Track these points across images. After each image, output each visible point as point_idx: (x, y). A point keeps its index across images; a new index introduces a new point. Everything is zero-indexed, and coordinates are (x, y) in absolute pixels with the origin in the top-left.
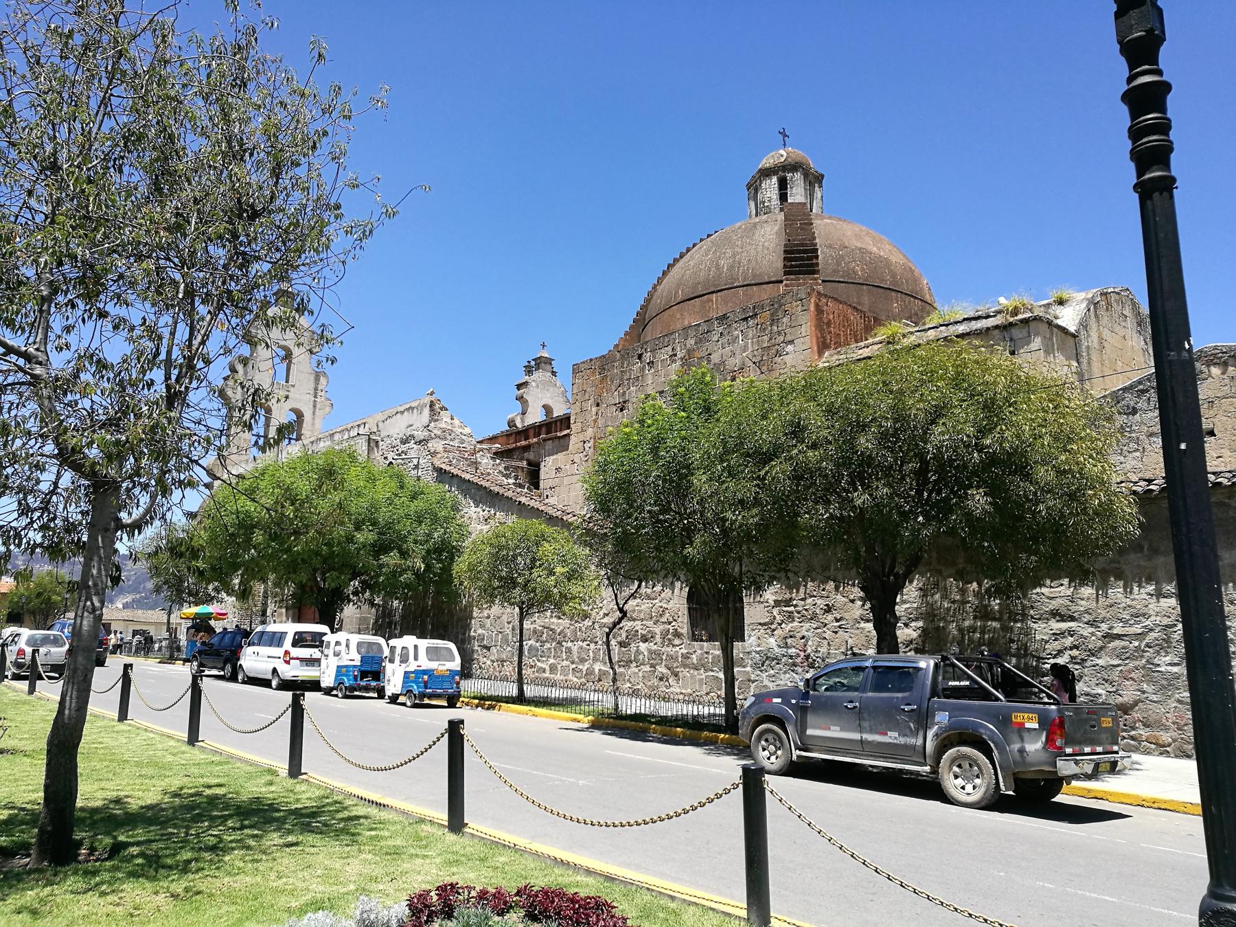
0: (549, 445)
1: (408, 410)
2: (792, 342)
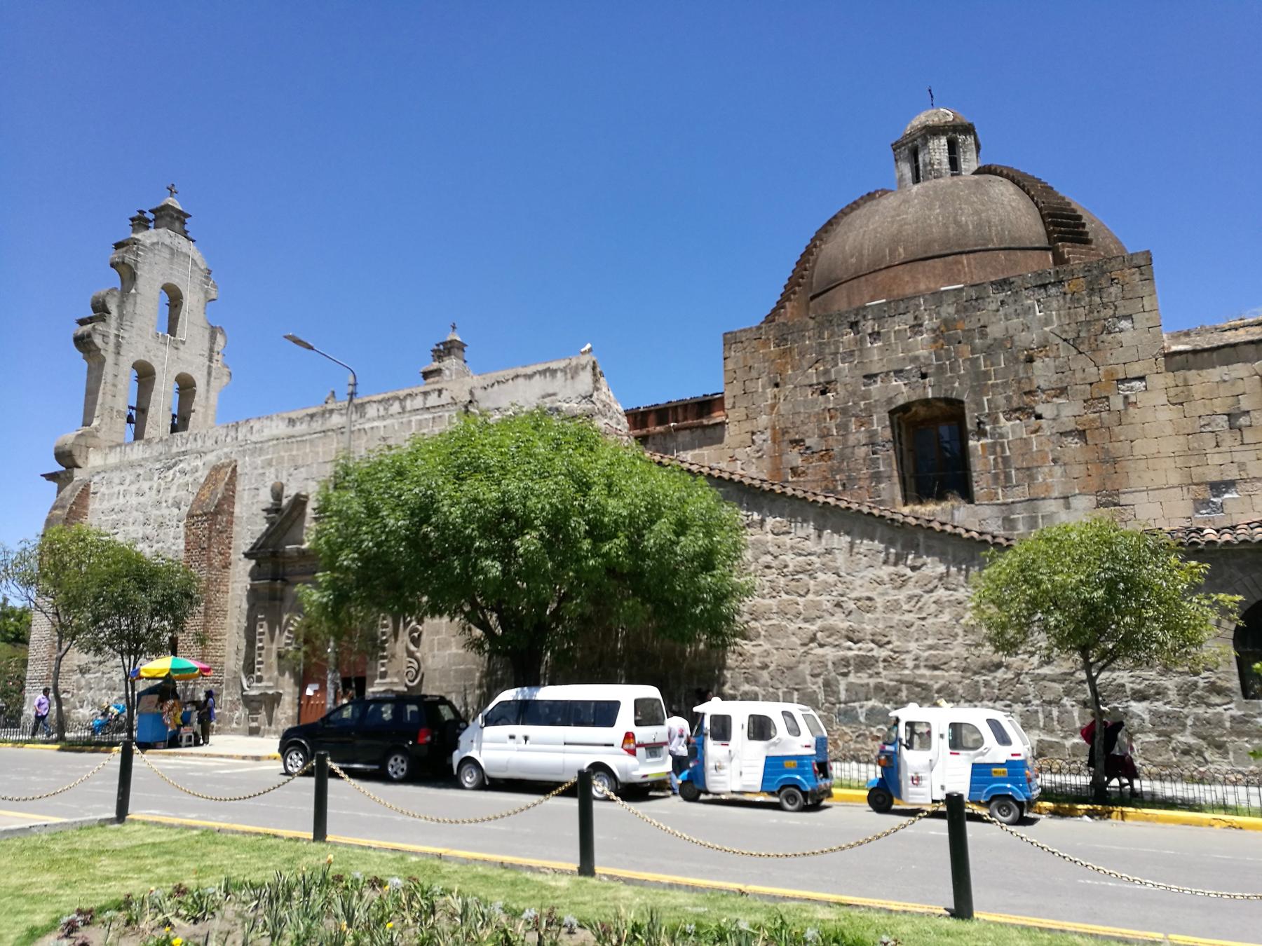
0: (684, 436)
1: (543, 373)
2: (1129, 317)
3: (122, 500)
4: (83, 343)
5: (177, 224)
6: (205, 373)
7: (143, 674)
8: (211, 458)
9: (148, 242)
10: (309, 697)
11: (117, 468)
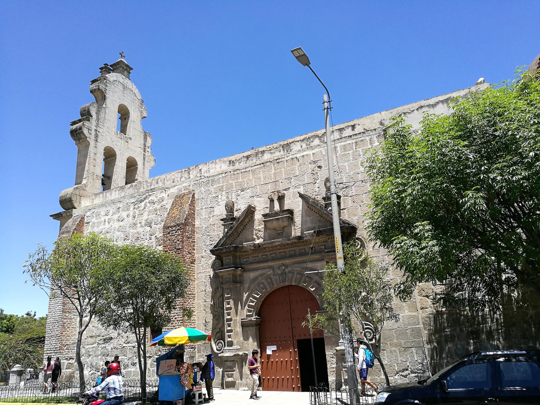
3: (107, 226)
4: (77, 135)
5: (126, 73)
6: (142, 158)
7: (167, 342)
8: (174, 191)
9: (111, 79)
10: (269, 356)
11: (103, 205)
